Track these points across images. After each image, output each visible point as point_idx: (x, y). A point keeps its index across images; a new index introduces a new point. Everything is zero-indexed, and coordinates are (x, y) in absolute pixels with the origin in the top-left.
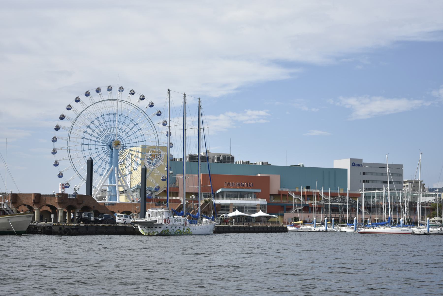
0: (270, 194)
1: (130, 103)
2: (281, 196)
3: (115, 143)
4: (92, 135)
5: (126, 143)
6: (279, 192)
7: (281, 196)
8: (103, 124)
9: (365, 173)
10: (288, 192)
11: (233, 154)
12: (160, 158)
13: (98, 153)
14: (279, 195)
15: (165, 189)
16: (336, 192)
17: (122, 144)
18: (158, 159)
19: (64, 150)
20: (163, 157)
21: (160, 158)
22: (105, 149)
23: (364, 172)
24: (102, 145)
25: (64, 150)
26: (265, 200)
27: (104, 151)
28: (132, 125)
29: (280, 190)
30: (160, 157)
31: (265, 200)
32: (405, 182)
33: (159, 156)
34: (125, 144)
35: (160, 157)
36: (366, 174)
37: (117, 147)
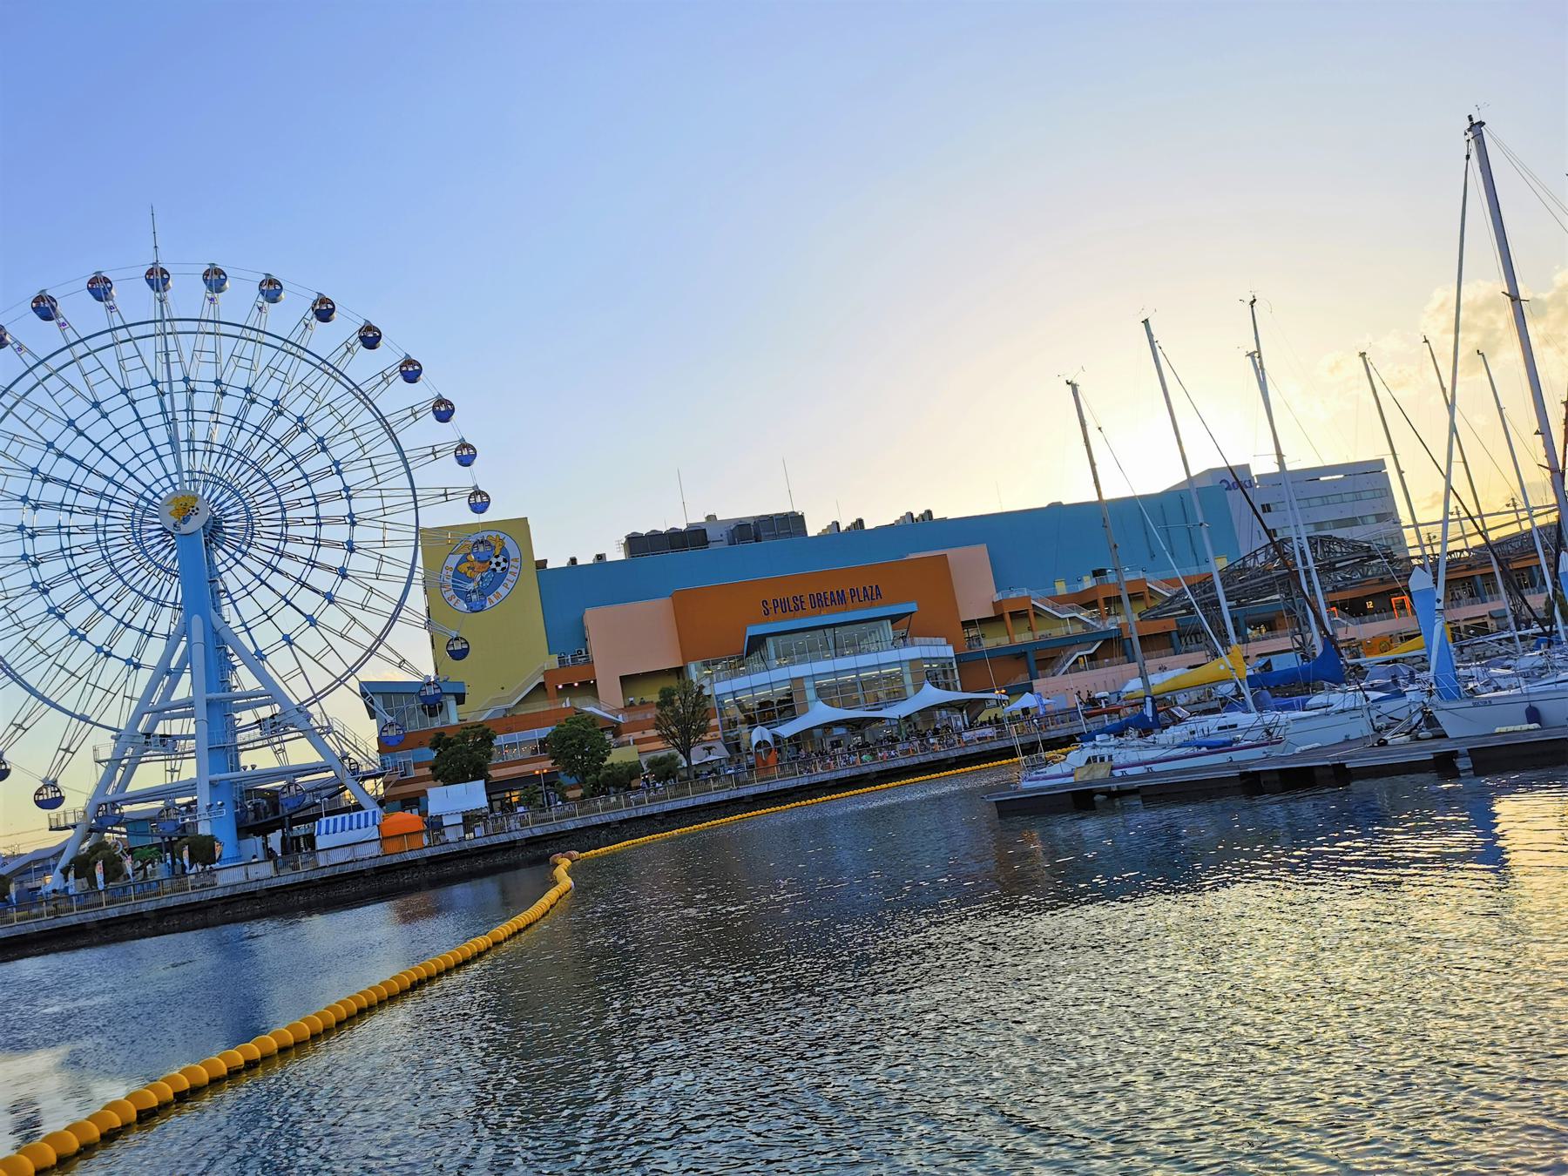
0: (963, 619)
1: (341, 374)
2: (1007, 617)
3: (172, 508)
4: (241, 428)
5: (160, 473)
6: (996, 605)
7: (1007, 617)
8: (306, 492)
9: (1268, 505)
10: (1028, 598)
11: (798, 509)
12: (503, 565)
13: (250, 589)
14: (998, 619)
15: (541, 679)
16: (1204, 570)
17: (171, 490)
18: (498, 569)
19: (391, 649)
20: (516, 560)
21: (503, 565)
22: (224, 562)
23: (1265, 503)
24: (168, 476)
25: (391, 649)
26: (943, 641)
27: (231, 562)
28: (230, 406)
29: (997, 598)
30: (505, 561)
31: (943, 641)
32: (605, 1099)
33: (500, 559)
34: (168, 476)
35: (505, 561)
36: (1272, 507)
37: (185, 521)
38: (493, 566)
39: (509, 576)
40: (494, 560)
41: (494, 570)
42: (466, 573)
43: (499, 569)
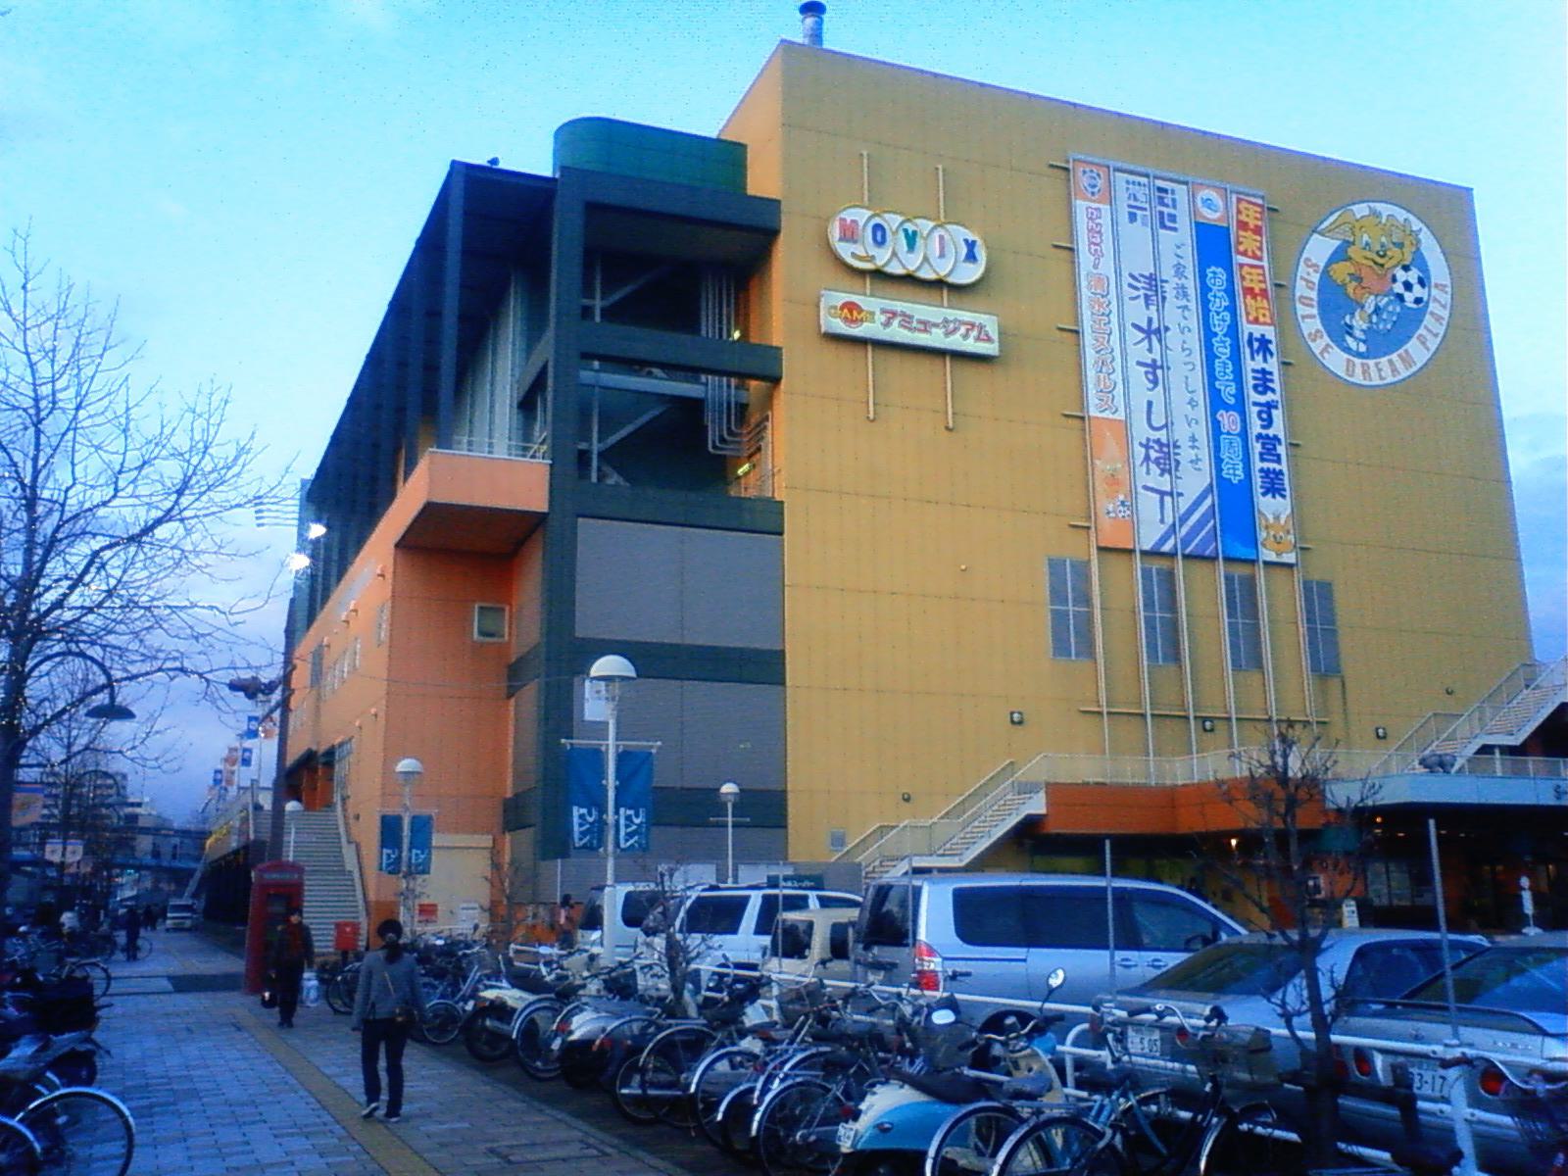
12: (1418, 291)
30: (1422, 282)
33: (1413, 276)
38: (1399, 288)
39: (1428, 320)
40: (1401, 275)
41: (1400, 297)
42: (1344, 285)
43: (1409, 297)
